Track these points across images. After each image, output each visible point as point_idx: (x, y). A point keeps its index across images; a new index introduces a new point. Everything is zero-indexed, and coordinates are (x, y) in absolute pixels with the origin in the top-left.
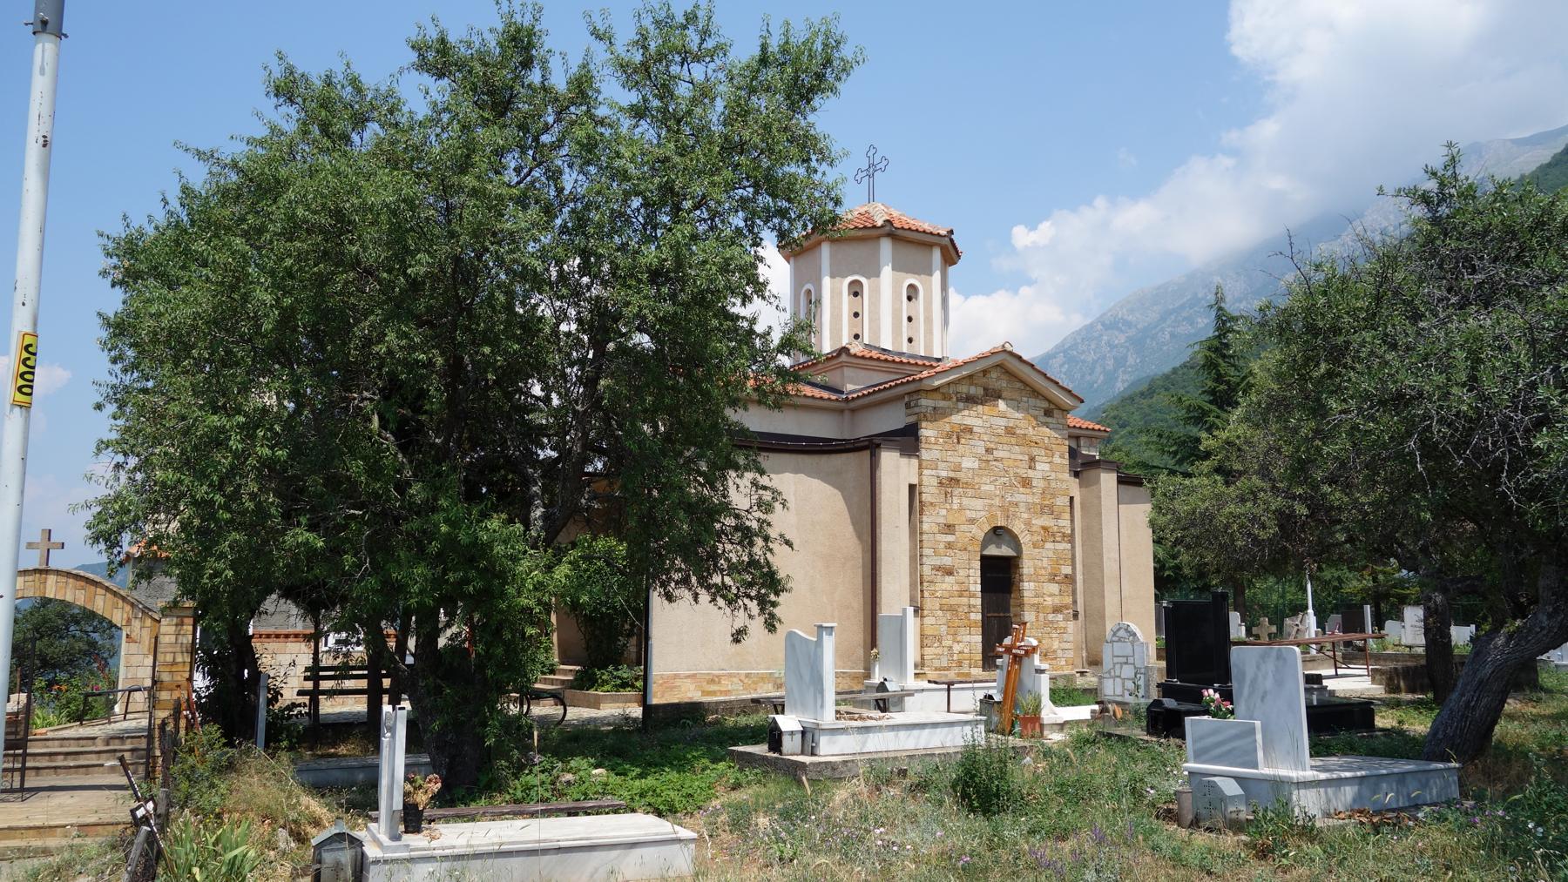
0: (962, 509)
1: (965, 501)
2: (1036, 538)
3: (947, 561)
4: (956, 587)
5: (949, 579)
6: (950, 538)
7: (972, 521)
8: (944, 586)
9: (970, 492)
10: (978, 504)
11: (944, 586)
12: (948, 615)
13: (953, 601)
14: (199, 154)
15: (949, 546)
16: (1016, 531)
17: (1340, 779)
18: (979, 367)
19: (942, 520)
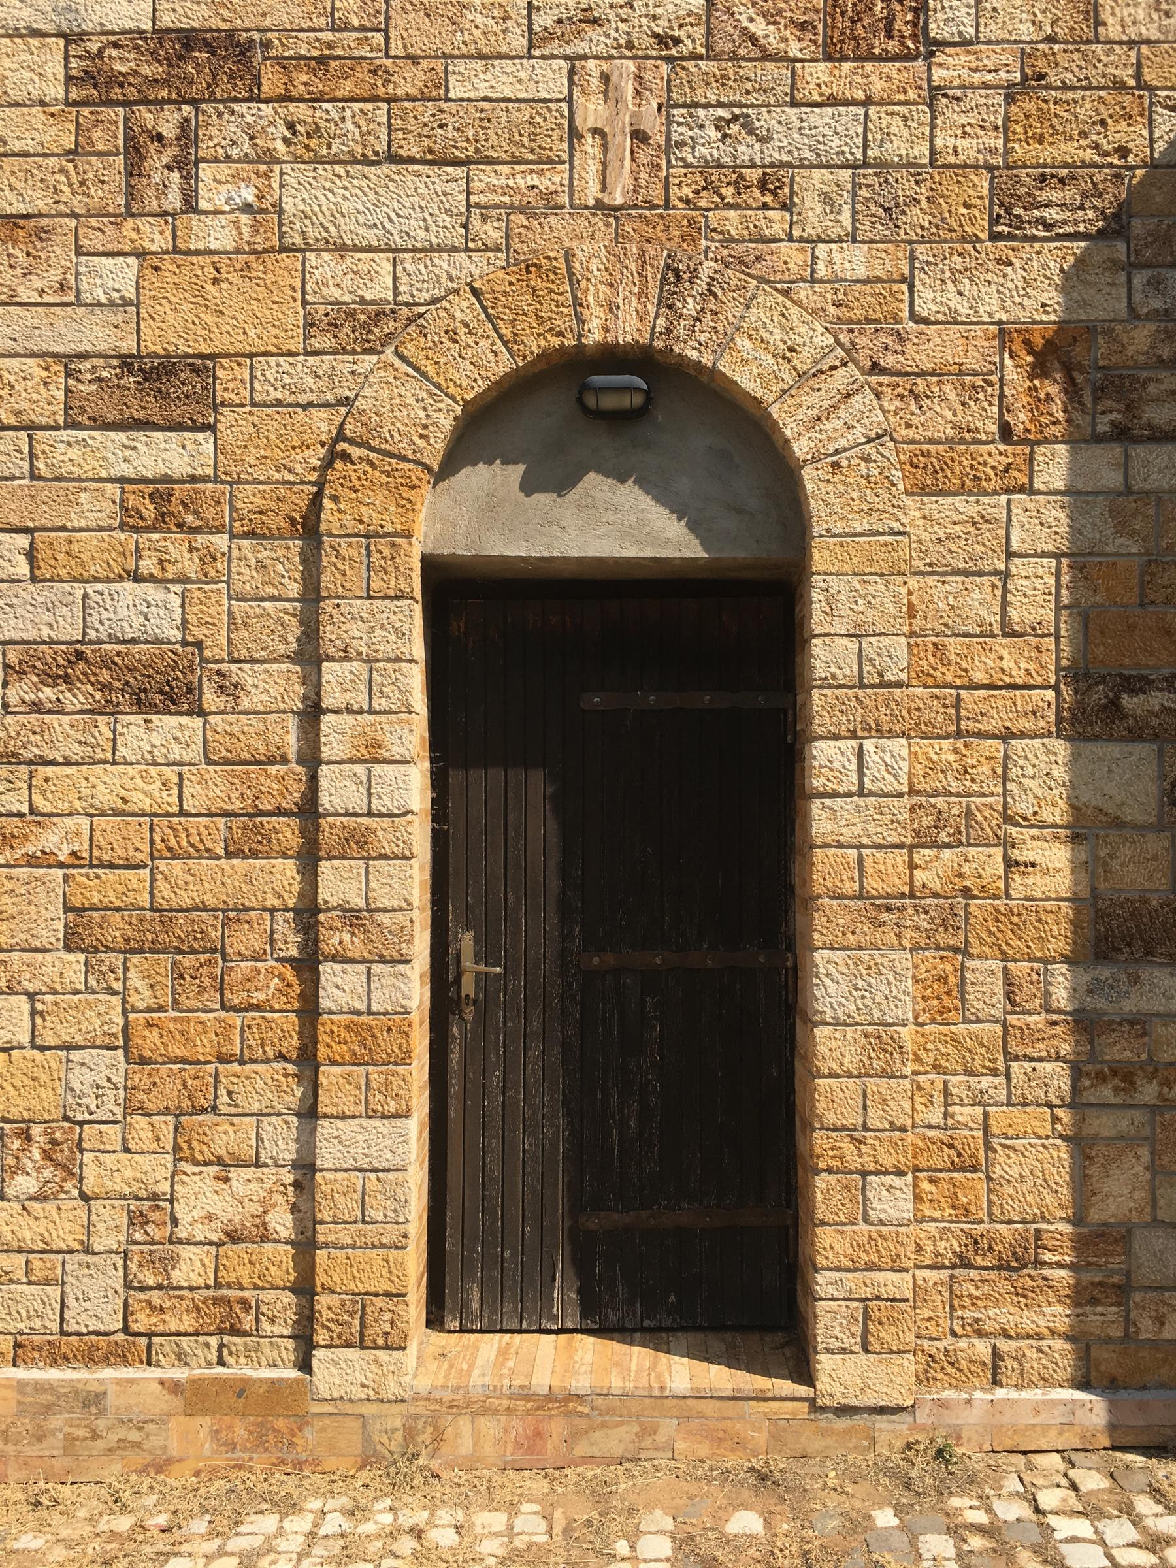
0: (273, 240)
1: (305, 194)
2: (939, 417)
3: (141, 614)
4: (209, 789)
5: (173, 733)
6: (169, 454)
7: (367, 327)
8: (106, 786)
9: (350, 125)
10: (419, 203)
11: (106, 786)
12: (142, 980)
13: (182, 883)
14: (1128, 1545)
15: (160, 506)
16: (748, 372)
17: (56, 1358)
18: (790, 989)
19: (98, 334)
